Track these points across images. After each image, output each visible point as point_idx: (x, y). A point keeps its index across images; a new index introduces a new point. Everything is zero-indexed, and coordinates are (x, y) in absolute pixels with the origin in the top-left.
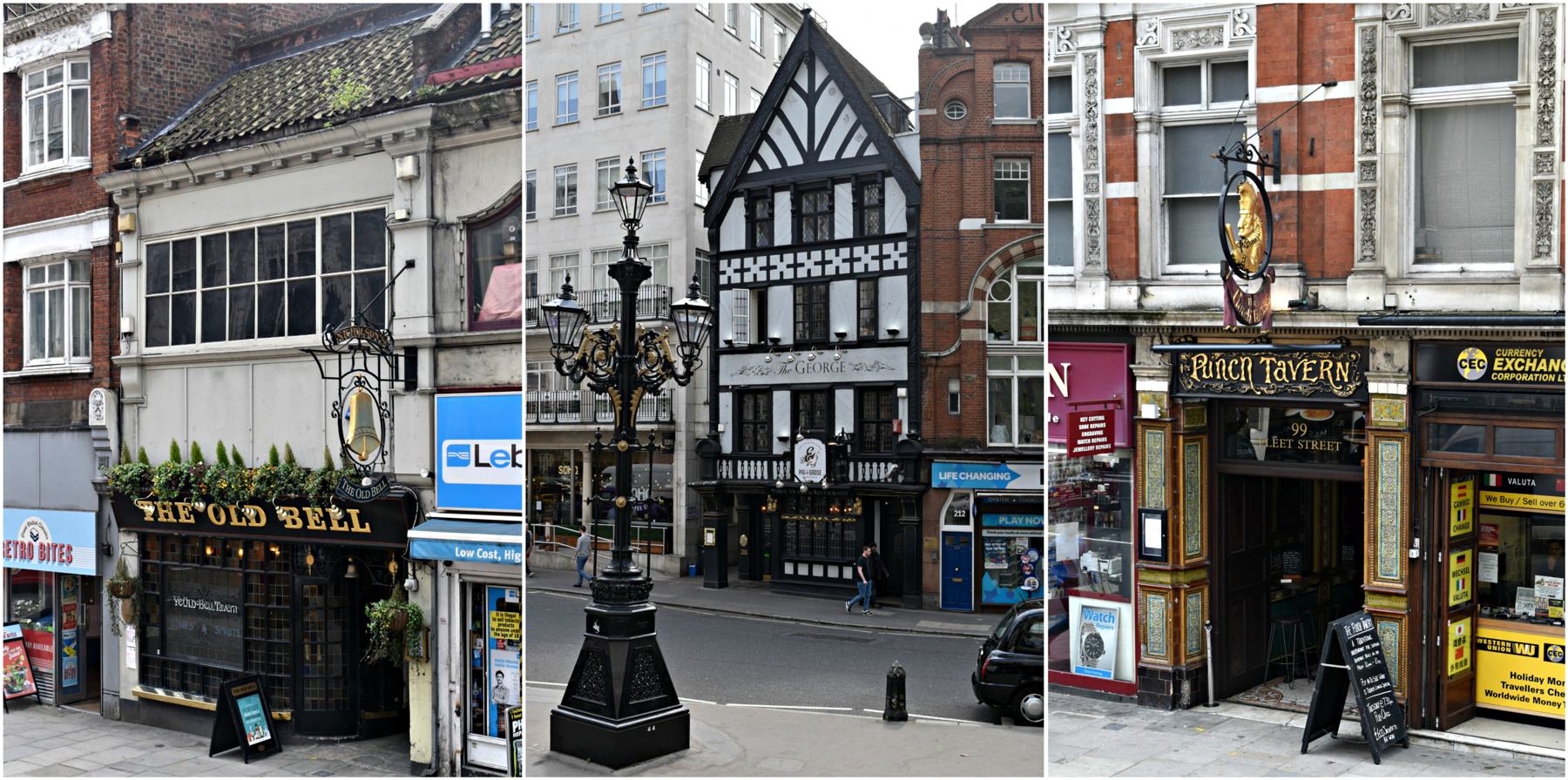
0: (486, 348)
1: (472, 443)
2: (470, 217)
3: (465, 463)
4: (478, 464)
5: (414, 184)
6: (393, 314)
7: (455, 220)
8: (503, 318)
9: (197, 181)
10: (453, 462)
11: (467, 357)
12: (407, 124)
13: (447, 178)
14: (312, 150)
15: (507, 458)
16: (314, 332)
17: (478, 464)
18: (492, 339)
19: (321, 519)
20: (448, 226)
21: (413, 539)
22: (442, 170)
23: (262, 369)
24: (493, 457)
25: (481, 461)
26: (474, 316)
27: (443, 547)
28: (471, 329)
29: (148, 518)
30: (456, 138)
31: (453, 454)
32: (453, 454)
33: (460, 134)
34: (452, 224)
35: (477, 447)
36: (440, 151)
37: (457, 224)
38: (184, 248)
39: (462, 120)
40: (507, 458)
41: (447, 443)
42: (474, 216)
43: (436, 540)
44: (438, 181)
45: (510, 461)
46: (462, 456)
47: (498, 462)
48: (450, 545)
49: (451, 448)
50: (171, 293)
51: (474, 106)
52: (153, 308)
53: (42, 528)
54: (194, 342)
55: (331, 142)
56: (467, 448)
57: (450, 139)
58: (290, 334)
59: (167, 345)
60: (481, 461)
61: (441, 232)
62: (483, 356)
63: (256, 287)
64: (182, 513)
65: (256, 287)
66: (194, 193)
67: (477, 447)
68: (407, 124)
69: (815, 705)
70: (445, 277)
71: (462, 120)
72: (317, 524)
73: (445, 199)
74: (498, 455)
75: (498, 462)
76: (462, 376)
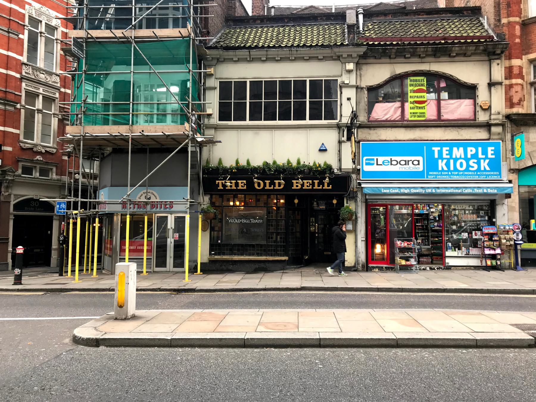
0: (377, 128)
1: (375, 158)
2: (370, 86)
3: (373, 164)
4: (377, 164)
5: (351, 73)
6: (341, 115)
7: (365, 87)
8: (379, 120)
9: (251, 59)
10: (367, 164)
11: (369, 131)
12: (355, 52)
13: (361, 73)
14: (310, 56)
15: (389, 162)
16: (219, 120)
17: (377, 164)
18: (381, 125)
19: (310, 184)
20: (362, 88)
21: (364, 188)
22: (360, 70)
23: (278, 133)
24: (383, 162)
25: (378, 164)
26: (369, 117)
27: (376, 189)
28: (368, 122)
29: (221, 187)
30: (367, 60)
31: (367, 161)
32: (367, 161)
33: (369, 59)
34: (363, 88)
35: (377, 159)
36: (360, 64)
37: (365, 88)
38: (241, 85)
39: (373, 54)
40: (389, 162)
41: (365, 158)
42: (372, 86)
43: (374, 187)
44: (358, 73)
45: (390, 163)
46: (372, 162)
47: (385, 164)
48: (380, 189)
49: (366, 160)
50: (292, 100)
51: (380, 50)
52: (222, 105)
53: (153, 194)
54: (245, 120)
55: (319, 54)
56: (373, 159)
57: (365, 60)
58: (234, 121)
59: (231, 121)
60: (378, 164)
61: (359, 90)
62: (375, 131)
63: (323, 101)
64: (240, 185)
65: (323, 101)
66: (289, 63)
67: (377, 159)
68: (355, 52)
69: (3, 262)
70: (361, 105)
71: (373, 54)
72: (242, 186)
73: (361, 80)
74: (385, 162)
75: (385, 164)
76: (367, 137)
